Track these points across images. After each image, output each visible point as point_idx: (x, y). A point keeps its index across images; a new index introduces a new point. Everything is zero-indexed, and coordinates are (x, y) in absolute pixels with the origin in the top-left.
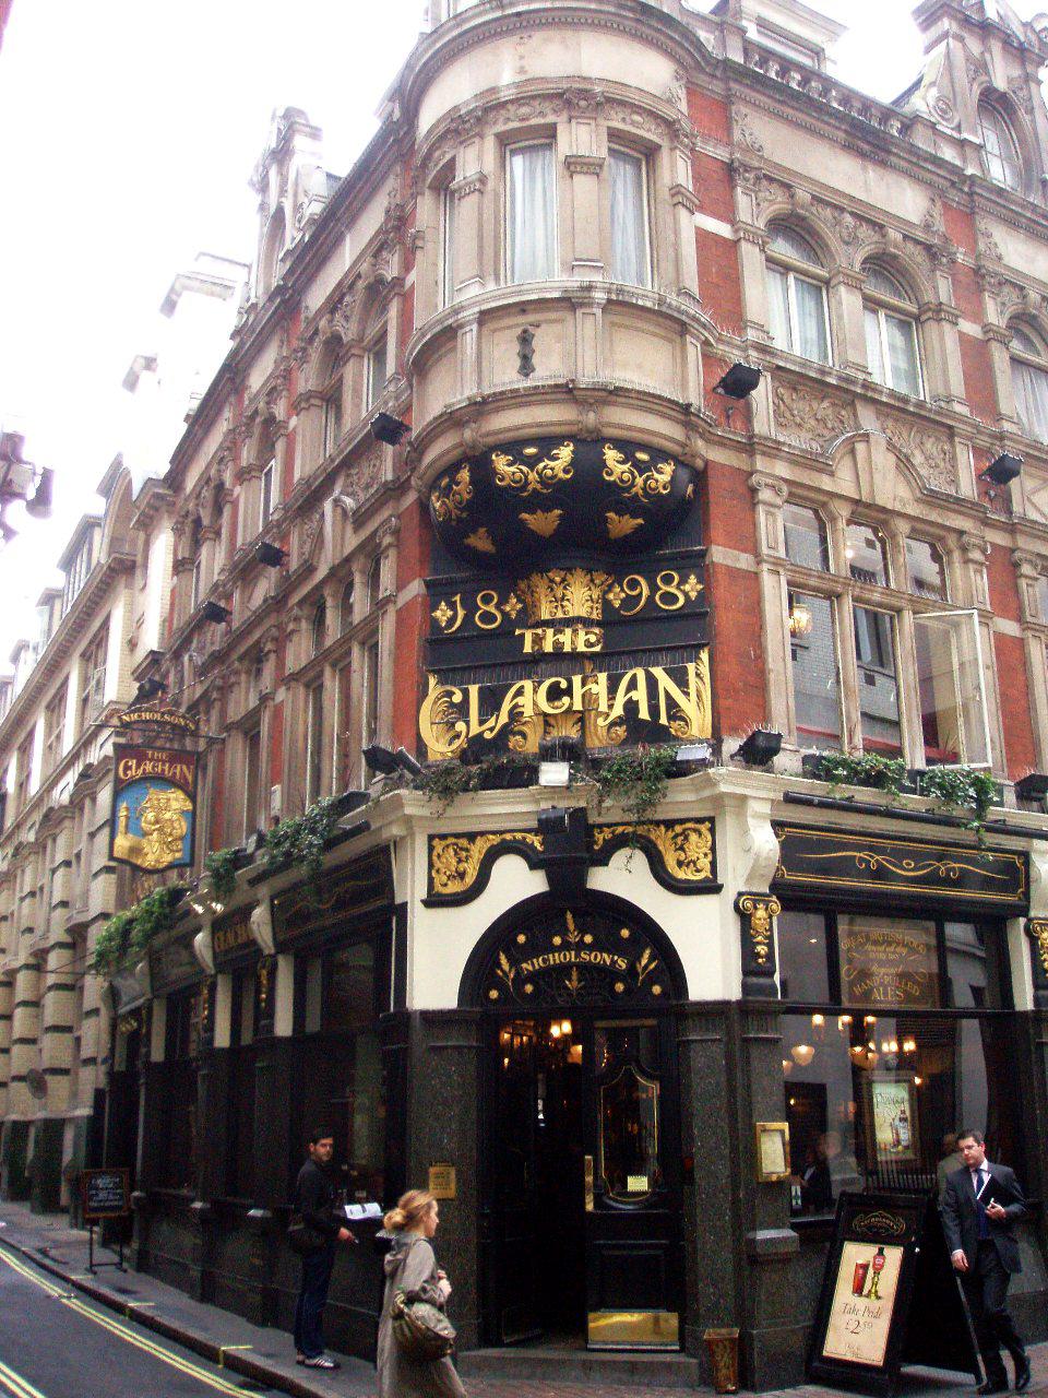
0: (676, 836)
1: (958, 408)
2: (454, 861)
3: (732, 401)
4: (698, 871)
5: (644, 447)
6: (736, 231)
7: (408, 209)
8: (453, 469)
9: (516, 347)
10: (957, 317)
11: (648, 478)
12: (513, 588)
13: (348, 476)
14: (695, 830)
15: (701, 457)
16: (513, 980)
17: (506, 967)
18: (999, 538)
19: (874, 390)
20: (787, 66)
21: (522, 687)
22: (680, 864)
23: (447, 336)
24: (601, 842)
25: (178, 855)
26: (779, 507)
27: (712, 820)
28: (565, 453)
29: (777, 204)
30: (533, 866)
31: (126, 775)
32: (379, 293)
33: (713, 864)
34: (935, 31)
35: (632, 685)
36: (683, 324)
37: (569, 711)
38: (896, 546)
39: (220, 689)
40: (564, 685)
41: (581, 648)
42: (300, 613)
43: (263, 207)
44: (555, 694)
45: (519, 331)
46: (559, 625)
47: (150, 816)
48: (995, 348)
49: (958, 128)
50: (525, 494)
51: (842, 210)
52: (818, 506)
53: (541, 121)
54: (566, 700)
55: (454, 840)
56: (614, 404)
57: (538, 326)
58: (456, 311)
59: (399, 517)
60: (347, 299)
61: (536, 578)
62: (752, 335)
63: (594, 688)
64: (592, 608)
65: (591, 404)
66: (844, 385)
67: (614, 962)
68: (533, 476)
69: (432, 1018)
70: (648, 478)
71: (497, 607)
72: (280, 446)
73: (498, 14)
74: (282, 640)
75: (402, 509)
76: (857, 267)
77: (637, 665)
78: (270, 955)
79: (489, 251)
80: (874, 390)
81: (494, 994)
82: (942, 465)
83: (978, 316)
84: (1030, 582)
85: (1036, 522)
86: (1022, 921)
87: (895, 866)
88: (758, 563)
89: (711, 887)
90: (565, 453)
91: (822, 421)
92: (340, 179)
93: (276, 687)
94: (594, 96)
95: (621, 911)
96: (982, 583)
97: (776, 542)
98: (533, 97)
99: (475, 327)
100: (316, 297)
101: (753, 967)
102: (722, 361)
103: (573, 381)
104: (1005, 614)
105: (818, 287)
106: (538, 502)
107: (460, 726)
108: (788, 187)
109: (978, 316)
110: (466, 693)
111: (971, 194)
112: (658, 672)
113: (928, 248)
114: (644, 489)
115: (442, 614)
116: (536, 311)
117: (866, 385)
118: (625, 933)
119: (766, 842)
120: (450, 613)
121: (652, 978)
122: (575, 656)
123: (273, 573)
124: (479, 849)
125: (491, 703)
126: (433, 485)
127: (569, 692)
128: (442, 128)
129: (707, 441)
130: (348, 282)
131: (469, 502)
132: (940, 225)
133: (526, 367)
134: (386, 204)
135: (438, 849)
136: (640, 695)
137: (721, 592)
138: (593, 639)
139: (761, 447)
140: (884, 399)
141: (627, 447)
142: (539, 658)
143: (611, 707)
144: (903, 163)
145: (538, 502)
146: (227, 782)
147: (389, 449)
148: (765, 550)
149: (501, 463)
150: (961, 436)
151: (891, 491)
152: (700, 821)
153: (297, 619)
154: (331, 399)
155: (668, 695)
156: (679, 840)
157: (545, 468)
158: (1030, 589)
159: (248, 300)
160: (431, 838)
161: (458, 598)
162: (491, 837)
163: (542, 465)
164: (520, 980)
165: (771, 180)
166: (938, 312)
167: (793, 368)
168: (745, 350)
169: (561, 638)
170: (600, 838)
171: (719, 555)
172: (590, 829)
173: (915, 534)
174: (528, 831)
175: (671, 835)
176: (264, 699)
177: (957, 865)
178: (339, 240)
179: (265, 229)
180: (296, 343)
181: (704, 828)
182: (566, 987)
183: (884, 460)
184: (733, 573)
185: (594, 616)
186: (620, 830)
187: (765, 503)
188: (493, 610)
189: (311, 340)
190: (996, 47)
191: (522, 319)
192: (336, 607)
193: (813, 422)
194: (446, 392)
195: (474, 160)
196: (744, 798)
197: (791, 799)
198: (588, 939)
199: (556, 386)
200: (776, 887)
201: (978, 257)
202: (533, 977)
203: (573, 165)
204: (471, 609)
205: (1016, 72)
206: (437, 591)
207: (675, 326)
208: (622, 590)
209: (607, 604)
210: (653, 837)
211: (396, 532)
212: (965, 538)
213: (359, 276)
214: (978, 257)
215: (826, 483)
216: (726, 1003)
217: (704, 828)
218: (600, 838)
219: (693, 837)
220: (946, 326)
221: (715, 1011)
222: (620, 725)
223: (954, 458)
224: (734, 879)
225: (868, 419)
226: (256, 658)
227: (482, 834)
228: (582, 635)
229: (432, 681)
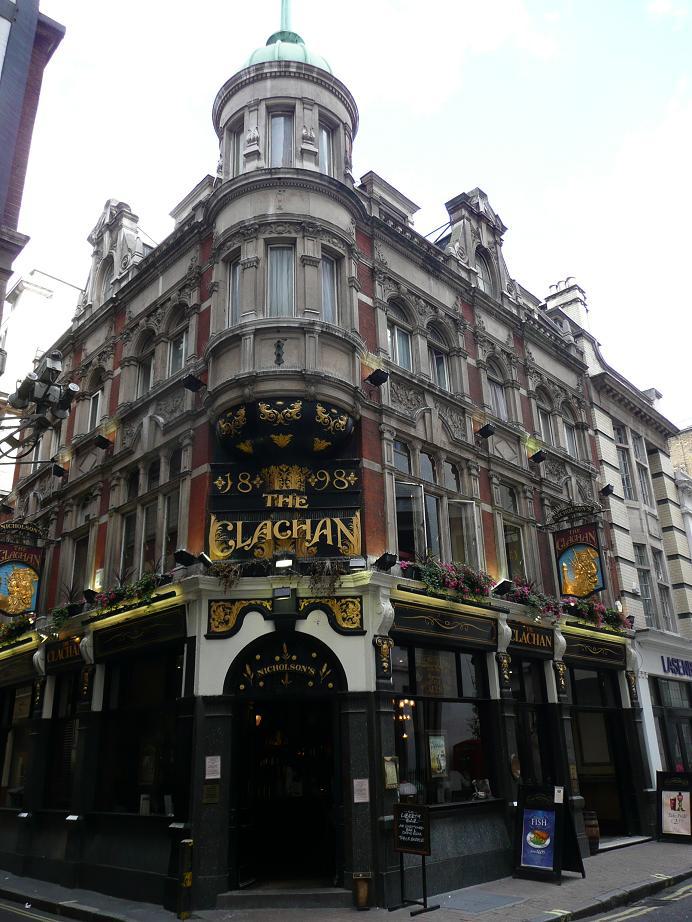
0: (342, 605)
1: (467, 400)
2: (222, 614)
5: (336, 407)
6: (374, 303)
7: (204, 269)
8: (235, 409)
13: (158, 405)
17: (249, 672)
18: (482, 464)
20: (397, 223)
22: (344, 619)
23: (234, 340)
27: (361, 597)
28: (298, 406)
29: (392, 291)
32: (181, 312)
33: (361, 620)
34: (456, 215)
35: (324, 526)
37: (290, 538)
39: (57, 513)
40: (288, 524)
41: (297, 506)
43: (96, 253)
44: (283, 529)
46: (286, 493)
49: (467, 264)
51: (420, 298)
52: (405, 444)
53: (288, 235)
54: (289, 532)
56: (323, 383)
58: (242, 327)
59: (194, 430)
60: (159, 311)
63: (304, 527)
68: (280, 416)
69: (209, 701)
71: (249, 481)
72: (108, 385)
73: (269, 177)
74: (106, 492)
75: (196, 426)
77: (326, 516)
78: (91, 664)
79: (260, 298)
83: (475, 356)
86: (494, 653)
88: (383, 469)
89: (360, 632)
90: (298, 406)
91: (411, 401)
92: (152, 248)
93: (102, 513)
94: (317, 227)
96: (476, 485)
98: (286, 223)
99: (252, 336)
100: (138, 307)
101: (381, 674)
102: (369, 368)
105: (407, 335)
106: (281, 430)
107: (231, 543)
108: (397, 284)
109: (475, 356)
110: (235, 526)
111: (473, 296)
112: (337, 520)
113: (455, 320)
115: (219, 483)
118: (314, 655)
119: (388, 608)
121: (328, 679)
122: (294, 509)
123: (101, 452)
124: (236, 609)
125: (248, 532)
126: (222, 415)
127: (291, 528)
128: (234, 231)
129: (362, 407)
131: (244, 427)
132: (460, 311)
133: (279, 360)
134: (189, 264)
135: (214, 608)
136: (328, 532)
137: (367, 482)
138: (304, 501)
141: (328, 406)
142: (274, 509)
143: (312, 537)
145: (281, 430)
146: (60, 569)
147: (189, 394)
149: (264, 408)
151: (440, 439)
153: (119, 479)
154: (144, 364)
156: (344, 606)
159: (85, 302)
160: (210, 601)
165: (390, 279)
166: (459, 353)
171: (366, 463)
172: (298, 599)
176: (90, 522)
178: (156, 278)
179: (99, 266)
180: (120, 330)
181: (356, 601)
183: (437, 423)
184: (372, 472)
186: (312, 601)
188: (247, 483)
189: (132, 330)
190: (484, 226)
191: (277, 335)
192: (145, 474)
194: (230, 370)
195: (252, 251)
198: (294, 657)
199: (296, 371)
200: (392, 633)
201: (476, 327)
202: (265, 678)
203: (306, 261)
204: (235, 481)
205: (491, 239)
206: (217, 471)
207: (350, 349)
209: (308, 484)
210: (330, 604)
211: (192, 438)
212: (470, 463)
213: (169, 299)
215: (412, 432)
216: (368, 693)
217: (356, 601)
219: (351, 606)
223: (465, 423)
224: (373, 627)
225: (430, 403)
226: (85, 500)
227: (239, 600)
228: (298, 498)
229: (213, 518)
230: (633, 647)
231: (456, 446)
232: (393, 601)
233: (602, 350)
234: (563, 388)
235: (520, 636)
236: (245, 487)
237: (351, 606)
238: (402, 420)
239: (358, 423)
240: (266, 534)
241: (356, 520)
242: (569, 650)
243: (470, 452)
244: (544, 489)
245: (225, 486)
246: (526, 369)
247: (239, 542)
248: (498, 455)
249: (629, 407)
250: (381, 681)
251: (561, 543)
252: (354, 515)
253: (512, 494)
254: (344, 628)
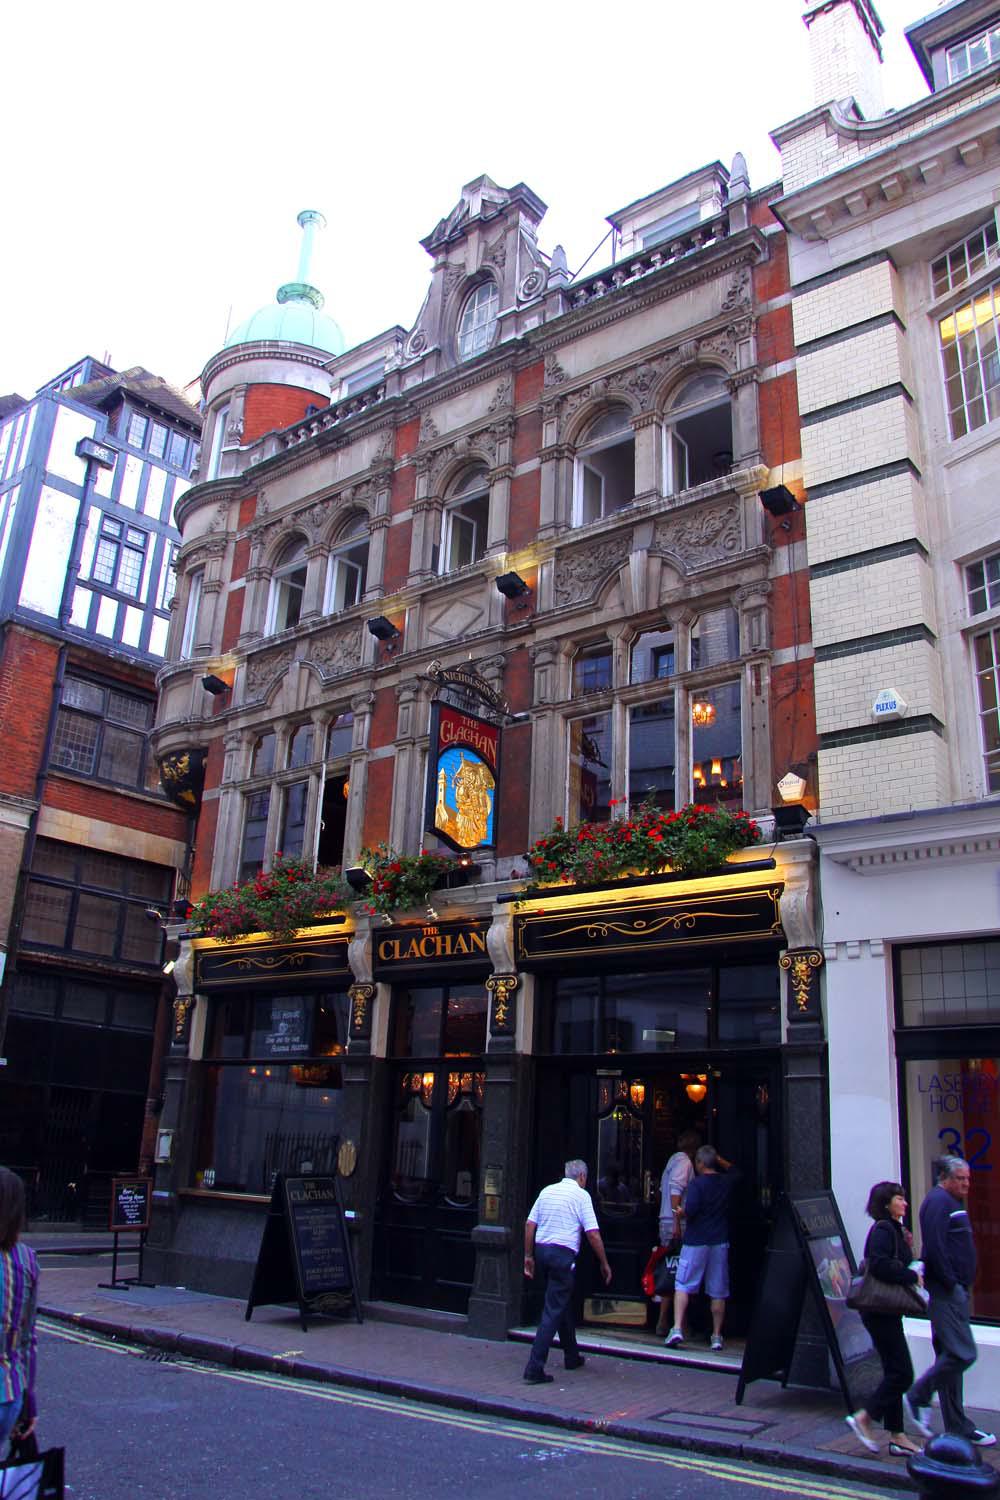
144: (358, 431)
233: (883, 52)
243: (360, 680)
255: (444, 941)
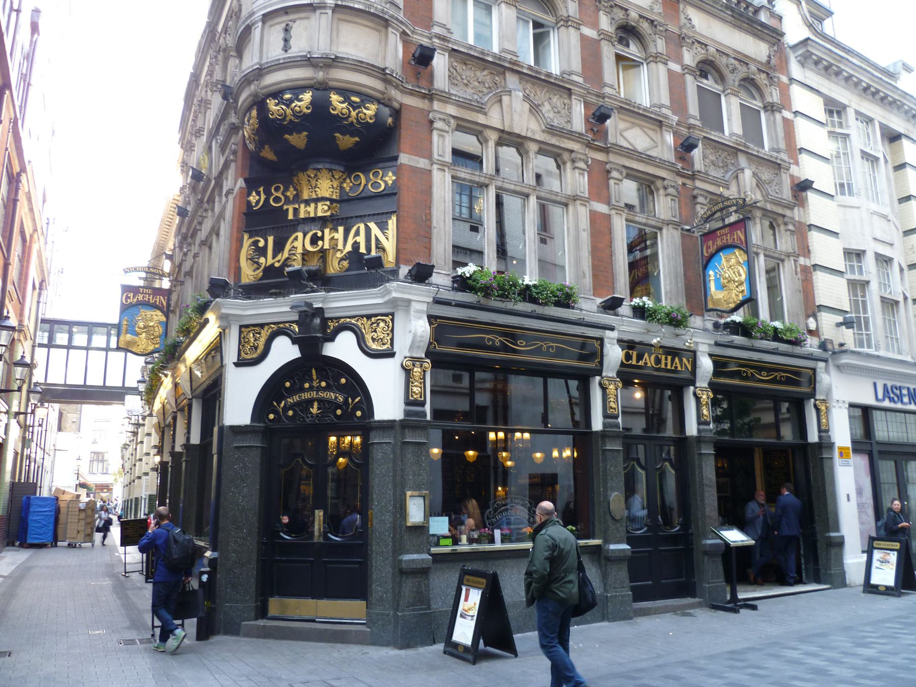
0: (373, 323)
3: (421, 68)
4: (384, 344)
9: (282, 35)
10: (667, 60)
11: (359, 112)
12: (291, 182)
14: (383, 320)
15: (396, 100)
16: (283, 408)
19: (518, 65)
21: (297, 236)
24: (332, 328)
25: (157, 346)
26: (447, 132)
27: (393, 314)
28: (307, 97)
29: (701, 54)
30: (293, 343)
31: (126, 301)
33: (392, 340)
35: (357, 233)
36: (387, 21)
38: (528, 157)
40: (320, 234)
41: (320, 214)
42: (207, 207)
44: (314, 240)
45: (284, 25)
47: (141, 324)
48: (604, 43)
50: (286, 123)
55: (253, 328)
56: (336, 67)
57: (294, 22)
61: (301, 175)
62: (436, 30)
63: (336, 236)
64: (333, 192)
65: (321, 67)
66: (498, 62)
67: (336, 398)
69: (237, 430)
70: (359, 112)
71: (283, 194)
76: (737, 83)
77: (361, 222)
80: (518, 65)
81: (271, 416)
82: (563, 112)
84: (616, 182)
85: (621, 147)
86: (598, 378)
87: (514, 344)
88: (432, 164)
89: (390, 354)
95: (341, 368)
97: (444, 151)
99: (260, 24)
103: (309, 52)
104: (600, 200)
107: (262, 260)
109: (595, 25)
110: (266, 241)
112: (372, 225)
114: (357, 119)
115: (253, 198)
116: (293, 13)
117: (515, 63)
119: (422, 328)
120: (257, 197)
121: (357, 407)
124: (265, 333)
125: (279, 247)
127: (322, 238)
129: (402, 92)
130: (229, 15)
136: (361, 239)
138: (326, 208)
139: (438, 97)
140: (525, 71)
141: (345, 92)
148: (435, 156)
149: (272, 104)
150: (576, 94)
152: (386, 315)
155: (377, 239)
157: (295, 106)
158: (616, 186)
160: (241, 327)
161: (261, 189)
162: (273, 326)
163: (294, 105)
164: (286, 409)
167: (463, 50)
168: (431, 39)
169: (308, 209)
170: (332, 325)
173: (541, 152)
174: (293, 322)
175: (369, 323)
177: (554, 345)
182: (311, 413)
184: (415, 170)
185: (334, 197)
187: (438, 129)
191: (285, 18)
193: (476, 84)
196: (409, 301)
197: (438, 302)
198: (323, 384)
202: (292, 407)
204: (268, 193)
207: (382, 22)
208: (351, 182)
210: (359, 324)
214: (680, 28)
215: (481, 119)
216: (394, 421)
217: (388, 319)
218: (332, 325)
219: (382, 324)
220: (572, 30)
221: (388, 426)
222: (345, 260)
223: (570, 108)
224: (402, 347)
227: (268, 324)
230: (827, 370)
231: (553, 135)
232: (711, 355)
234: (743, 60)
235: (640, 357)
236: (277, 200)
237: (382, 324)
238: (463, 104)
239: (397, 113)
240: (296, 248)
241: (392, 223)
242: (716, 373)
243: (578, 142)
244: (698, 184)
245: (258, 202)
246: (680, 40)
247: (268, 260)
248: (625, 144)
249: (877, 97)
250: (702, 427)
251: (708, 247)
252: (390, 218)
253: (772, 227)
254: (373, 350)
255: (666, 359)
